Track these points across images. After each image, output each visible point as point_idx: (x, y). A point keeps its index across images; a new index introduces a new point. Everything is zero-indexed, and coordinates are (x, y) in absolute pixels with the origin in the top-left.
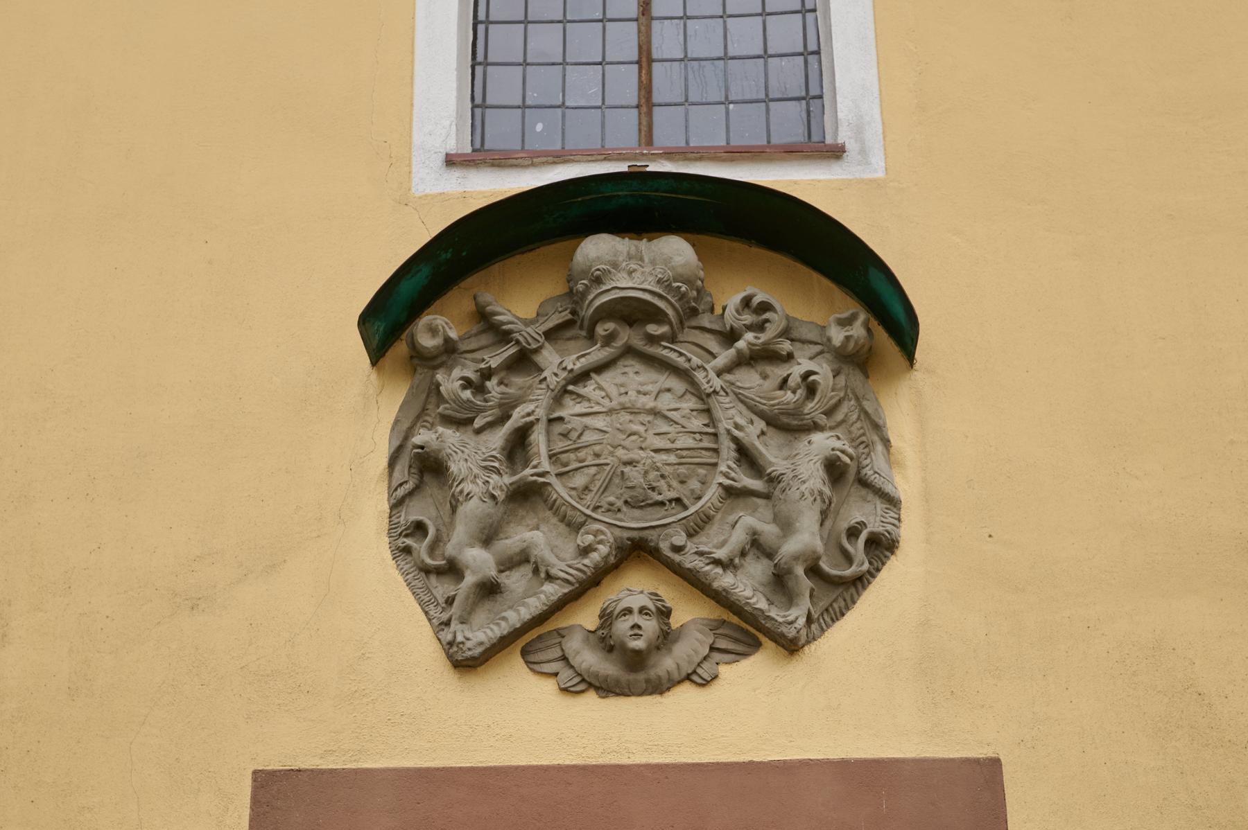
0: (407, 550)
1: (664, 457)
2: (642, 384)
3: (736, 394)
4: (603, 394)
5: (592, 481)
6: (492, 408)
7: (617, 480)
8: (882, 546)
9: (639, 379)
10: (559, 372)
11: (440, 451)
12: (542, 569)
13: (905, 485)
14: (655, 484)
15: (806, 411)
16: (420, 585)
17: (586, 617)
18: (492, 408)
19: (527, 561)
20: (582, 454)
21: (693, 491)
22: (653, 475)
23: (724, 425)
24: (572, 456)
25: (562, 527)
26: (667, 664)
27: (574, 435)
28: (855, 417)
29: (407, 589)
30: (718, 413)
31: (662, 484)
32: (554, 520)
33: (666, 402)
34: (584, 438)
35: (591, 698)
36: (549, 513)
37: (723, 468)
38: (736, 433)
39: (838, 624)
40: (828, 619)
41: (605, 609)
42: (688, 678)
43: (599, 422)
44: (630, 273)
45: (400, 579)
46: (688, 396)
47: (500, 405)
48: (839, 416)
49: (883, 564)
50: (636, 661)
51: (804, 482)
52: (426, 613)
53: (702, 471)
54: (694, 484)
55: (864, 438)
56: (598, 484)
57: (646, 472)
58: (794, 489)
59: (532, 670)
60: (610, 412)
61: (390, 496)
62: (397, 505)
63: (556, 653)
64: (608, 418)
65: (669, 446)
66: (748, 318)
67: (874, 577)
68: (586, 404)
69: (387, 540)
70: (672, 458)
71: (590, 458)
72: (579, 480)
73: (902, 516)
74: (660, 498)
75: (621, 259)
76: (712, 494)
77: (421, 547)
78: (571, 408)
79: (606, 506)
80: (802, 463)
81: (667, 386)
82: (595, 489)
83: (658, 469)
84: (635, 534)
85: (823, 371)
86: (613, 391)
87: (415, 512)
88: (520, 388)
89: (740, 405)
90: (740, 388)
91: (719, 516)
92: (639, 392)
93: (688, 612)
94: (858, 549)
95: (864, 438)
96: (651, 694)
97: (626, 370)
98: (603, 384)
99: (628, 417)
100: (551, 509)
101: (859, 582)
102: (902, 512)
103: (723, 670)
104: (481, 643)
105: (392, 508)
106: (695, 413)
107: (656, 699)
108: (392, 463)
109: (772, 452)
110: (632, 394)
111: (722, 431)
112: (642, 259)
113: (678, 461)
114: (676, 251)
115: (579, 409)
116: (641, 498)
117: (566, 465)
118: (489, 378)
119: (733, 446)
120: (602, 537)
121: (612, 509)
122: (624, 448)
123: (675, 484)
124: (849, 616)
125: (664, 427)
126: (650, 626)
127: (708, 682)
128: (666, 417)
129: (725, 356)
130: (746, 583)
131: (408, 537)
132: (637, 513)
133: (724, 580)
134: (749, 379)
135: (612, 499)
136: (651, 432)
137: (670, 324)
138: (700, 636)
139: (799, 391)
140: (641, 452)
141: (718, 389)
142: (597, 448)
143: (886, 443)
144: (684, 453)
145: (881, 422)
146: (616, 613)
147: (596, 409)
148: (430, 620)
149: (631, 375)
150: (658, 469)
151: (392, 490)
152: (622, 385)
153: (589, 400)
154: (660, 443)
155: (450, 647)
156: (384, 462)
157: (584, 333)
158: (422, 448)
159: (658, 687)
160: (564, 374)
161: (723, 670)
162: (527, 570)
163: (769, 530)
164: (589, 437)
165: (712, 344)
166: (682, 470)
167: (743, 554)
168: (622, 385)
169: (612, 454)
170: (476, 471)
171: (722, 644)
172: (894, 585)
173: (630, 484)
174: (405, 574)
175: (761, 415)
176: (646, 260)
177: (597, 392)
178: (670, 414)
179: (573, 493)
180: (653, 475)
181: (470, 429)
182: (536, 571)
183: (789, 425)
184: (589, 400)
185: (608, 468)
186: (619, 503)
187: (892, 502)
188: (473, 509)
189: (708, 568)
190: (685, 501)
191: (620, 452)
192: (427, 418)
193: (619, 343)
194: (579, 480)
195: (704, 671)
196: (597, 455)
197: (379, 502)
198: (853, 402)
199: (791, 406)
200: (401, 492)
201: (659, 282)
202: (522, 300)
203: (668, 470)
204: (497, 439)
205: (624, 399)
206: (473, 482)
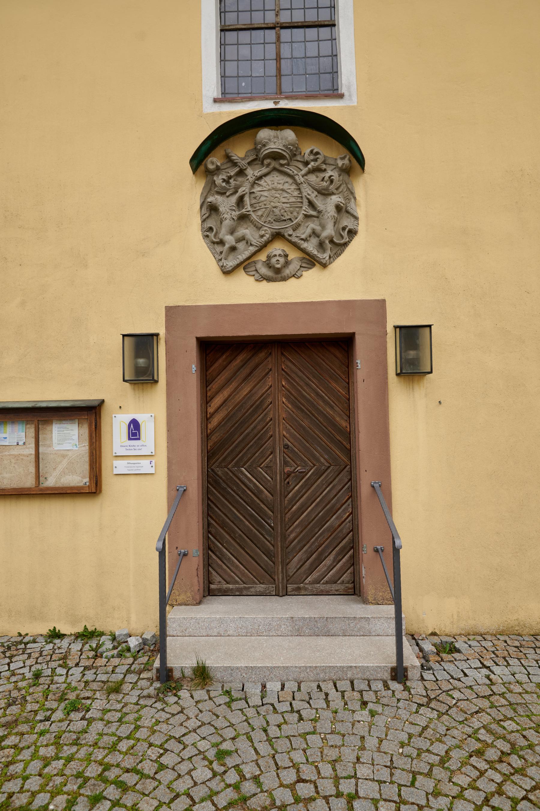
0: (207, 236)
1: (286, 205)
2: (279, 180)
3: (308, 183)
5: (264, 213)
6: (232, 189)
7: (271, 213)
8: (352, 233)
13: (360, 212)
17: (263, 257)
20: (260, 204)
23: (305, 194)
24: (257, 205)
25: (255, 228)
26: (287, 272)
27: (258, 198)
28: (345, 190)
30: (303, 190)
32: (252, 226)
33: (286, 186)
34: (261, 199)
35: (265, 282)
36: (250, 224)
38: (308, 197)
42: (293, 276)
43: (265, 194)
44: (275, 143)
45: (206, 245)
46: (293, 184)
47: (234, 188)
48: (340, 190)
50: (278, 271)
53: (297, 209)
54: (295, 214)
60: (269, 190)
61: (201, 218)
62: (203, 221)
65: (287, 201)
66: (312, 157)
67: (350, 243)
70: (288, 205)
72: (260, 213)
74: (284, 218)
76: (301, 217)
77: (212, 235)
78: (257, 189)
80: (328, 205)
84: (277, 231)
86: (270, 183)
87: (210, 223)
93: (293, 255)
94: (345, 234)
99: (275, 192)
101: (346, 245)
103: (304, 273)
107: (284, 282)
109: (319, 203)
111: (304, 196)
117: (255, 208)
119: (307, 201)
121: (270, 222)
123: (289, 214)
124: (342, 255)
125: (286, 195)
126: (282, 260)
128: (286, 192)
129: (305, 170)
130: (311, 246)
132: (278, 223)
133: (304, 245)
134: (312, 178)
135: (270, 219)
137: (287, 159)
138: (297, 263)
142: (265, 202)
144: (292, 204)
147: (265, 189)
151: (202, 216)
156: (199, 207)
159: (284, 279)
160: (254, 177)
163: (318, 228)
164: (263, 199)
165: (301, 166)
166: (291, 209)
169: (270, 204)
171: (304, 265)
174: (207, 244)
175: (316, 190)
182: (247, 243)
183: (325, 193)
186: (272, 220)
187: (356, 218)
190: (293, 219)
193: (271, 166)
194: (260, 213)
195: (298, 274)
196: (265, 205)
197: (197, 221)
200: (204, 217)
202: (240, 151)
204: (234, 199)
205: (273, 186)
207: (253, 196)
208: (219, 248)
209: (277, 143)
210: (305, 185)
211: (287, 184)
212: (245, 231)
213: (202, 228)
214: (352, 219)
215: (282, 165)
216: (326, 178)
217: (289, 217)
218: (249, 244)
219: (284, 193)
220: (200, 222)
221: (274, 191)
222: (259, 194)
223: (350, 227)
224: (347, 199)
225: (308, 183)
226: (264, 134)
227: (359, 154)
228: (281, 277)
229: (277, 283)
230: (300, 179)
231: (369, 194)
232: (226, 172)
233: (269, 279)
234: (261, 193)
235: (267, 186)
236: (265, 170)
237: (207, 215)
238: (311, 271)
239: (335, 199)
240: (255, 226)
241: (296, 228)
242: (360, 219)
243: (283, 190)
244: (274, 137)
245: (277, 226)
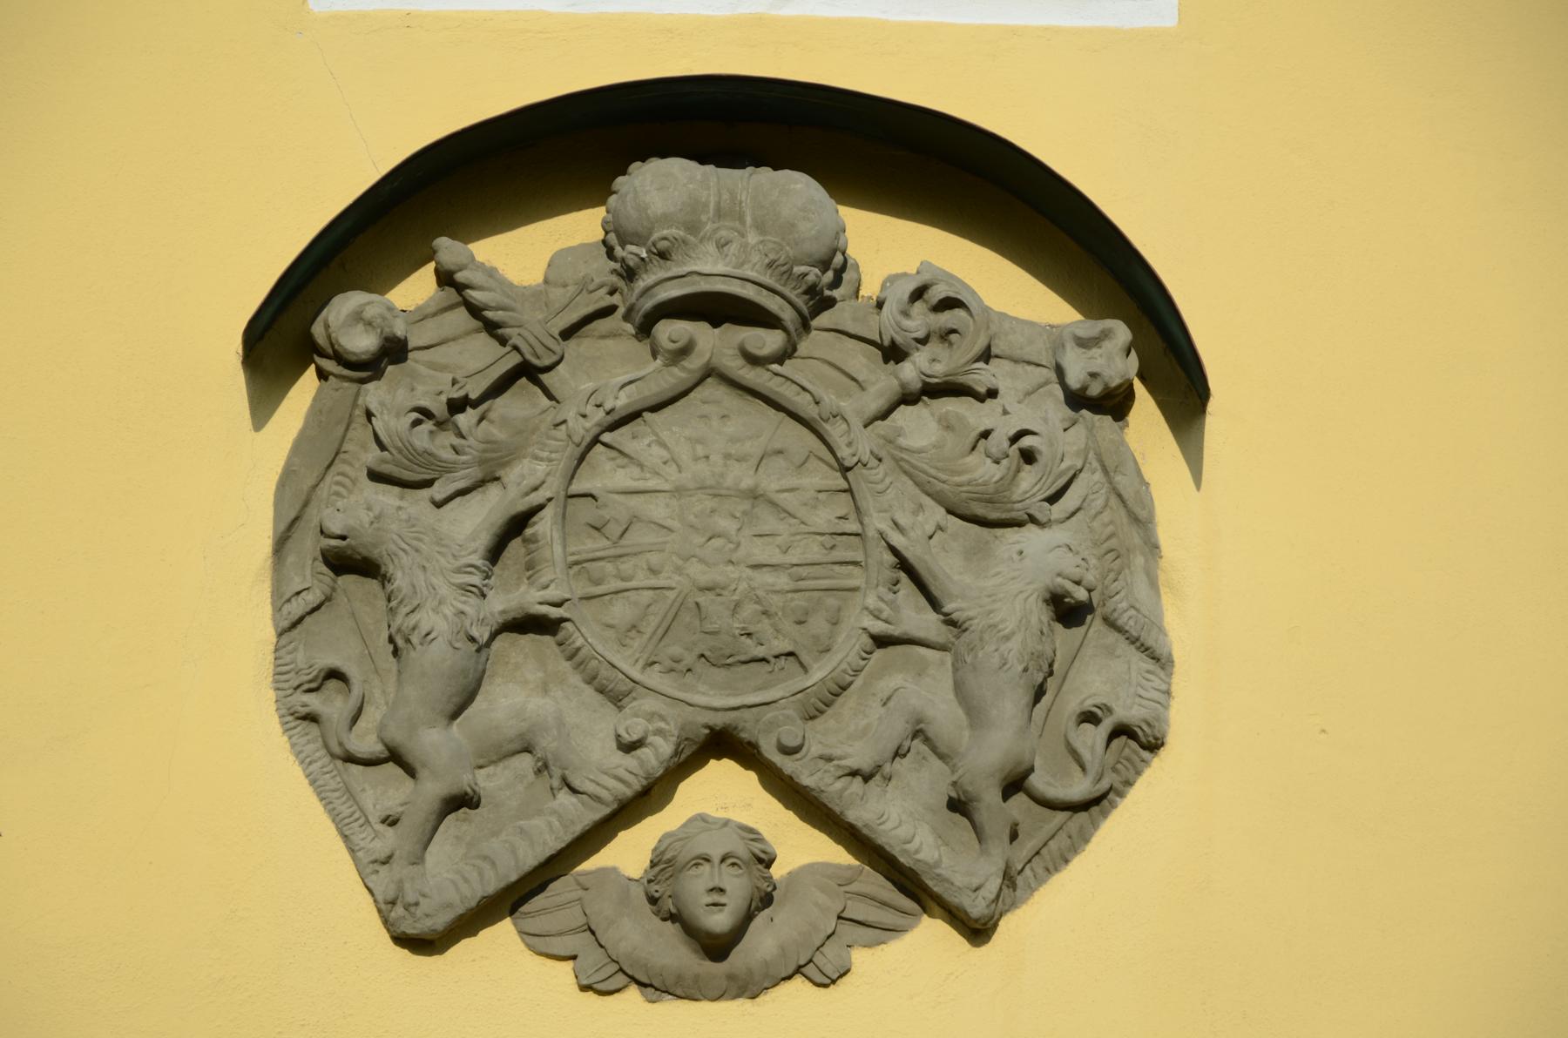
0: (311, 718)
1: (767, 578)
2: (733, 440)
3: (897, 460)
4: (664, 453)
5: (644, 616)
6: (467, 465)
7: (686, 617)
8: (1139, 740)
9: (731, 428)
10: (589, 409)
11: (375, 546)
12: (557, 772)
13: (1181, 629)
14: (752, 629)
15: (1015, 497)
16: (333, 785)
17: (629, 853)
18: (467, 465)
19: (528, 750)
20: (626, 566)
21: (816, 638)
22: (749, 609)
23: (877, 522)
24: (609, 567)
25: (589, 691)
26: (762, 942)
27: (614, 530)
28: (1100, 502)
29: (310, 789)
30: (868, 502)
31: (764, 627)
32: (575, 679)
33: (771, 481)
34: (630, 539)
35: (633, 996)
36: (566, 666)
37: (871, 601)
38: (897, 540)
39: (1057, 880)
40: (1040, 871)
41: (663, 853)
42: (799, 970)
43: (658, 509)
44: (722, 245)
45: (298, 771)
46: (813, 463)
47: (481, 462)
48: (1069, 501)
49: (1139, 773)
50: (717, 947)
51: (1007, 638)
52: (345, 838)
53: (831, 601)
54: (818, 624)
55: (1113, 543)
56: (653, 621)
57: (737, 605)
58: (990, 648)
59: (530, 947)
60: (678, 491)
61: (277, 610)
62: (289, 628)
63: (574, 917)
64: (674, 502)
65: (778, 558)
66: (920, 320)
67: (1121, 795)
68: (636, 471)
69: (272, 695)
70: (782, 581)
71: (641, 574)
72: (620, 611)
73: (1174, 689)
74: (760, 652)
75: (704, 218)
76: (848, 646)
77: (332, 705)
78: (604, 475)
79: (668, 663)
80: (1003, 582)
81: (778, 446)
82: (649, 631)
83: (758, 601)
84: (719, 720)
85: (1046, 416)
86: (684, 452)
87: (330, 646)
88: (520, 432)
89: (905, 478)
90: (902, 449)
91: (859, 681)
92: (727, 456)
93: (800, 847)
94: (1091, 739)
95: (1113, 543)
96: (734, 998)
97: (707, 409)
98: (665, 435)
99: (710, 503)
100: (570, 658)
101: (1095, 804)
102: (1176, 679)
103: (861, 958)
104: (450, 905)
105: (280, 635)
106: (822, 496)
107: (740, 1006)
108: (281, 543)
109: (948, 555)
110: (716, 458)
111: (871, 533)
112: (741, 219)
113: (792, 585)
114: (793, 191)
115: (623, 478)
116: (728, 652)
117: (597, 583)
118: (462, 410)
119: (889, 558)
120: (662, 725)
121: (674, 668)
122: (701, 561)
123: (788, 625)
124: (1077, 863)
125: (769, 522)
126: (738, 888)
127: (834, 982)
128: (773, 504)
129: (883, 381)
130: (904, 816)
131: (312, 696)
132: (720, 675)
133: (865, 808)
134: (919, 427)
135: (676, 650)
136: (747, 532)
137: (785, 329)
138: (821, 898)
139: (1005, 462)
140: (731, 568)
141: (865, 459)
142: (654, 558)
143: (1153, 548)
144: (803, 571)
145: (1142, 514)
146: (500, 331)
147: (652, 483)
148: (352, 851)
149: (715, 423)
150: (758, 601)
151: (280, 599)
152: (699, 441)
153: (641, 466)
154: (763, 552)
155: (386, 908)
156: (266, 544)
157: (629, 328)
158: (343, 538)
159: (748, 987)
160: (600, 415)
161: (861, 958)
162: (525, 763)
163: (944, 713)
164: (640, 537)
165: (861, 360)
166: (800, 601)
167: (898, 754)
168: (699, 441)
169: (679, 570)
170: (444, 590)
171: (858, 910)
172: (1155, 791)
173: (709, 627)
174: (305, 762)
175: (938, 498)
176: (749, 220)
177: (656, 449)
178: (782, 498)
179: (610, 633)
180: (749, 609)
181: (425, 493)
182: (543, 768)
183: (988, 517)
184: (641, 466)
185: (671, 595)
186: (689, 659)
187: (1160, 660)
188: (438, 656)
189: (839, 785)
190: (805, 657)
191: (696, 570)
192: (347, 469)
193: (695, 363)
194: (620, 611)
195: (829, 959)
196: (654, 571)
197: (257, 626)
198: (1098, 476)
199: (991, 488)
200: (297, 608)
201: (770, 265)
202: (526, 255)
203: (776, 601)
204: (475, 520)
205: (702, 468)
206: (436, 611)
207: (583, 509)
208: (385, 791)
209: (733, 248)
210: (882, 469)
211: (780, 462)
212: (521, 690)
213: (279, 673)
214: (1141, 663)
215: (753, 360)
216: (999, 441)
217: (786, 646)
218: (554, 774)
219: (763, 511)
220: (268, 633)
221: (697, 496)
222: (619, 508)
223: (1127, 711)
224: (1116, 555)
225: (897, 460)
226: (661, 185)
227: (1175, 329)
228: (731, 977)
229: (705, 1006)
230: (857, 442)
231: (1229, 536)
232: (432, 366)
233: (655, 986)
234: (634, 501)
235: (671, 469)
236: (659, 378)
237: (312, 598)
238: (896, 949)
239: (1044, 554)
240: (591, 680)
241: (818, 706)
242: (1179, 669)
243: (754, 495)
244: (719, 214)
245: (713, 699)
